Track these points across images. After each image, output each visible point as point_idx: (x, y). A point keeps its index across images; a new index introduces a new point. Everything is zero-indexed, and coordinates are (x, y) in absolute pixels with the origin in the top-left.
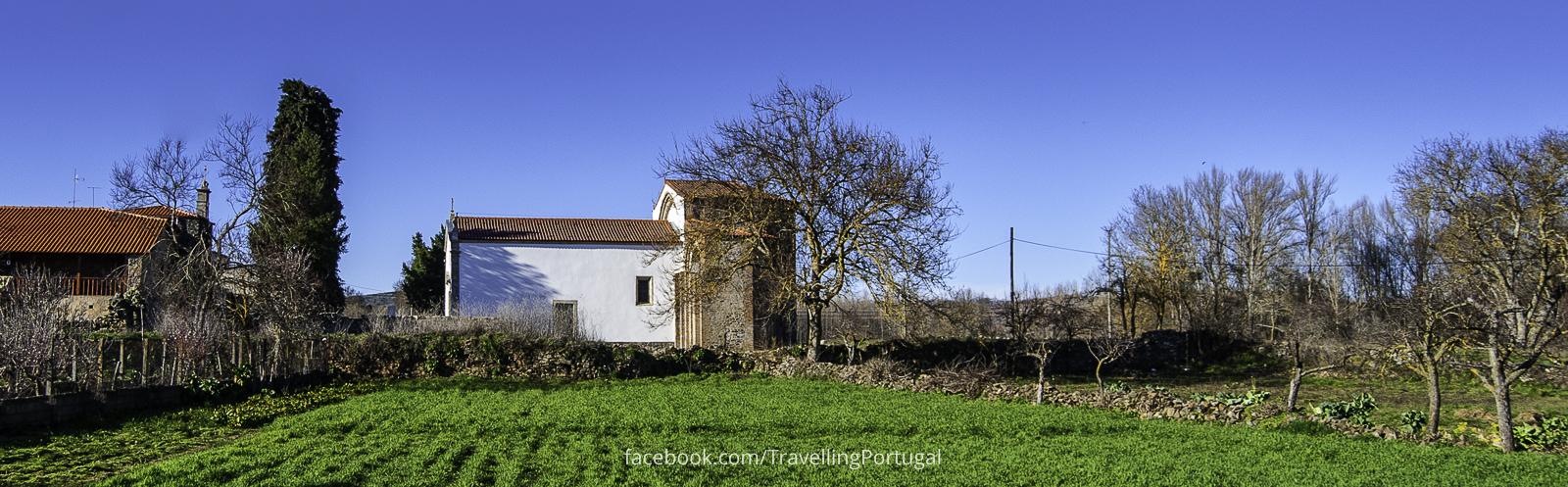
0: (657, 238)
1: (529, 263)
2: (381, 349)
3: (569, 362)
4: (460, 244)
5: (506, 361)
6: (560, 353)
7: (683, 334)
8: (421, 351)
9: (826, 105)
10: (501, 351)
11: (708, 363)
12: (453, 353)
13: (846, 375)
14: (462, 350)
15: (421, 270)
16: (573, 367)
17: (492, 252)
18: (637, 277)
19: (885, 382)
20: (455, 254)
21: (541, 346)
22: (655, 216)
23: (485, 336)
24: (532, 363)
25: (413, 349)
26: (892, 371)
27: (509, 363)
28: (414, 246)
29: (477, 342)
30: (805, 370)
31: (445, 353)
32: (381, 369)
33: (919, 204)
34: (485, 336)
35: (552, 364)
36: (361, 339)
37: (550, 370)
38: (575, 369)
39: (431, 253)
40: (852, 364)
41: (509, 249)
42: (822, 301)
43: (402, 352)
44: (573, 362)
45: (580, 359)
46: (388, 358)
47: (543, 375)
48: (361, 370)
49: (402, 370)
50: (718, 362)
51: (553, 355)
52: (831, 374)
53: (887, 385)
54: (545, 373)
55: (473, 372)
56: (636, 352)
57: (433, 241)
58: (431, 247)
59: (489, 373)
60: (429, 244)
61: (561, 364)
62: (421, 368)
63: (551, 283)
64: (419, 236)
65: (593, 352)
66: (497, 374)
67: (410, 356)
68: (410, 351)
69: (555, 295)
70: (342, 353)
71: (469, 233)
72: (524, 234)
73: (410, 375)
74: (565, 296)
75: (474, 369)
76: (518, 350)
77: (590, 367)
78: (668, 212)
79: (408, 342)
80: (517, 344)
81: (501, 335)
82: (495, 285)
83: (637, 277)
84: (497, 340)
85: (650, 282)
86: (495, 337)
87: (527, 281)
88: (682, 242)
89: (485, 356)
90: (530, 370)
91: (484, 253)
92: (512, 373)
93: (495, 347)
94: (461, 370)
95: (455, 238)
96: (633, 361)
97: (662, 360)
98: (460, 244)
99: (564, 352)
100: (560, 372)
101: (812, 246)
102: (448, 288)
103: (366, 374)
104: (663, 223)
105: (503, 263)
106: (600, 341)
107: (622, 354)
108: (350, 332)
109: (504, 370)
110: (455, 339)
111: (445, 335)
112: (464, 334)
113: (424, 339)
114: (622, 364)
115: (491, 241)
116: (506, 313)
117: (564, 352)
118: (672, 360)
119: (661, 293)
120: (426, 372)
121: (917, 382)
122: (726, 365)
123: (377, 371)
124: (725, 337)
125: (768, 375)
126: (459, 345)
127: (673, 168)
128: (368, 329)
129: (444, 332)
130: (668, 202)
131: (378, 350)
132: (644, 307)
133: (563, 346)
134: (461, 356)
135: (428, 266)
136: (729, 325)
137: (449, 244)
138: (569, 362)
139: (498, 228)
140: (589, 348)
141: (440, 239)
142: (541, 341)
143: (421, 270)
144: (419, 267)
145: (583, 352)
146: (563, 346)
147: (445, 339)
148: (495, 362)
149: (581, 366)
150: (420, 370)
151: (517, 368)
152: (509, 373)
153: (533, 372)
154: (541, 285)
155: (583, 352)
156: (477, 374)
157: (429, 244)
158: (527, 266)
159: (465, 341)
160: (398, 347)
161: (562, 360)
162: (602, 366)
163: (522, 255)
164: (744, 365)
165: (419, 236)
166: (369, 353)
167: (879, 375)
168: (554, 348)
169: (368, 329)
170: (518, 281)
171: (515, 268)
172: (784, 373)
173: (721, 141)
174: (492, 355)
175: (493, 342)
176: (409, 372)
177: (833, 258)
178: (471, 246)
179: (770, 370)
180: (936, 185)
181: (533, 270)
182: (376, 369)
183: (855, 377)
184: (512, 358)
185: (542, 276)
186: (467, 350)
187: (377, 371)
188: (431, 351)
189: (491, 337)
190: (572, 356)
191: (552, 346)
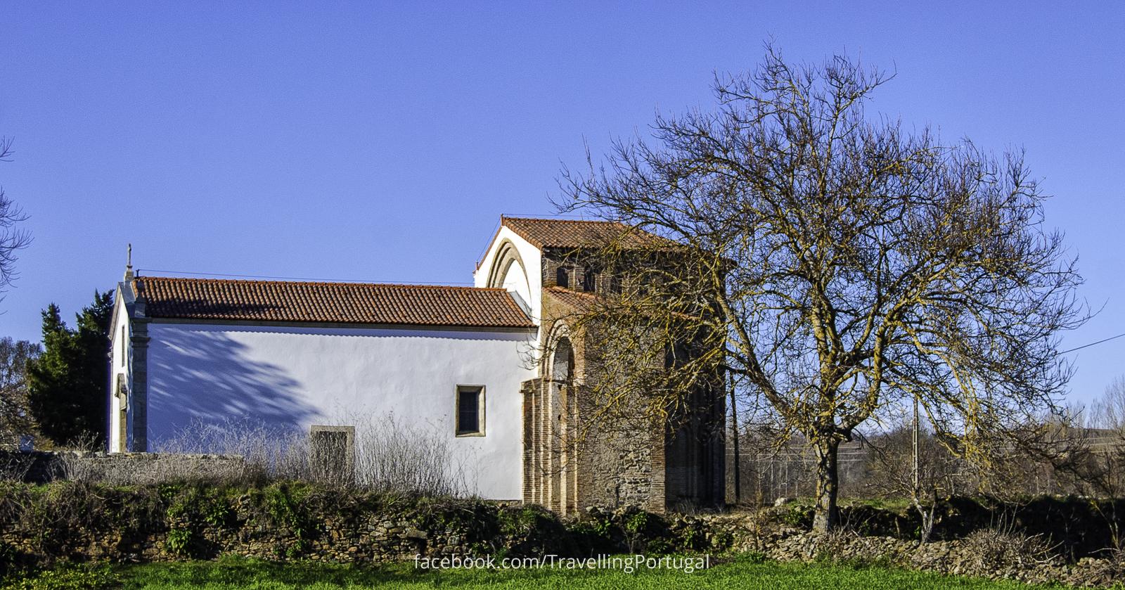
0: (491, 318)
1: (272, 362)
2: (89, 509)
3: (423, 534)
4: (150, 327)
5: (311, 532)
6: (408, 519)
7: (537, 488)
8: (159, 514)
9: (848, 90)
10: (304, 514)
11: (654, 538)
12: (217, 517)
13: (926, 558)
14: (233, 513)
15: (60, 369)
16: (430, 542)
17: (206, 341)
18: (459, 387)
19: (1009, 570)
20: (139, 343)
21: (374, 505)
22: (481, 280)
23: (274, 488)
24: (358, 536)
25: (146, 510)
26: (1023, 552)
27: (316, 536)
28: (46, 329)
29: (260, 498)
30: (839, 550)
31: (203, 517)
32: (88, 544)
33: (1009, 264)
34: (274, 488)
35: (394, 539)
36: (52, 491)
37: (388, 548)
38: (434, 546)
39: (78, 342)
40: (929, 541)
41: (234, 335)
42: (840, 431)
43: (127, 515)
44: (430, 535)
45: (443, 529)
46: (100, 526)
47: (376, 557)
48: (52, 549)
49: (124, 547)
50: (670, 535)
51: (394, 521)
52: (894, 556)
53: (1013, 576)
54: (380, 553)
55: (252, 553)
56: (539, 518)
57: (80, 320)
58: (77, 329)
59: (282, 553)
60: (72, 325)
61: (409, 538)
62: (160, 544)
63: (309, 396)
64: (54, 310)
65: (465, 517)
66: (297, 555)
67: (142, 523)
68: (142, 513)
69: (314, 417)
70: (17, 518)
71: (162, 306)
72: (259, 308)
73: (140, 557)
74: (333, 419)
75: (254, 547)
76: (333, 513)
77: (460, 543)
78: (505, 274)
79: (136, 498)
80: (332, 501)
81: (302, 486)
82: (212, 400)
83: (459, 387)
84: (297, 495)
85: (481, 396)
86: (291, 489)
87: (266, 392)
88: (537, 327)
89: (274, 523)
90: (353, 549)
91: (193, 343)
92: (322, 553)
93: (293, 507)
94: (231, 548)
95: (140, 313)
96: (533, 533)
97: (575, 532)
98: (150, 327)
99: (415, 516)
100: (407, 551)
101: (820, 336)
102: (117, 405)
103: (61, 554)
104: (496, 294)
105: (224, 360)
106: (473, 498)
107: (515, 520)
108: (27, 480)
109: (308, 549)
110: (220, 493)
111: (203, 485)
112: (236, 484)
113: (166, 490)
114: (514, 538)
115: (203, 321)
116: (224, 454)
117: (415, 516)
118: (593, 534)
119: (503, 416)
120: (170, 551)
121: (1074, 571)
122: (683, 540)
123: (80, 550)
124: (617, 492)
125: (764, 558)
126: (227, 504)
127: (584, 197)
128: (61, 475)
129: (201, 480)
130: (505, 258)
131: (84, 511)
132: (469, 440)
133: (413, 506)
134: (232, 522)
135: (72, 364)
136: (623, 470)
137: (122, 319)
138: (423, 534)
139: (213, 298)
140: (458, 511)
141: (102, 316)
142: (375, 498)
143: (60, 369)
144: (54, 364)
145: (448, 517)
146: (413, 506)
147: (203, 492)
148: (292, 534)
149: (443, 541)
150: (158, 548)
151: (331, 543)
152: (318, 553)
153: (359, 551)
154: (289, 399)
155: (448, 517)
156: (259, 555)
157: (72, 325)
158: (269, 366)
159: (237, 497)
160: (119, 507)
161: (411, 531)
162: (480, 541)
163: (259, 347)
164: (714, 541)
165: (54, 310)
166: (68, 515)
167: (997, 560)
168: (398, 509)
169: (61, 475)
170: (248, 391)
171: (242, 369)
172: (798, 555)
173: (672, 155)
174: (287, 520)
175: (288, 497)
176: (138, 551)
177: (857, 357)
178: (172, 329)
179: (765, 548)
180: (1036, 231)
181: (280, 374)
182: (79, 545)
183: (945, 561)
184: (323, 528)
185: (294, 383)
186: (242, 513)
187: (80, 550)
188: (179, 514)
189: (284, 489)
190: (428, 524)
191: (394, 506)
